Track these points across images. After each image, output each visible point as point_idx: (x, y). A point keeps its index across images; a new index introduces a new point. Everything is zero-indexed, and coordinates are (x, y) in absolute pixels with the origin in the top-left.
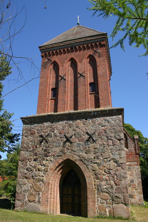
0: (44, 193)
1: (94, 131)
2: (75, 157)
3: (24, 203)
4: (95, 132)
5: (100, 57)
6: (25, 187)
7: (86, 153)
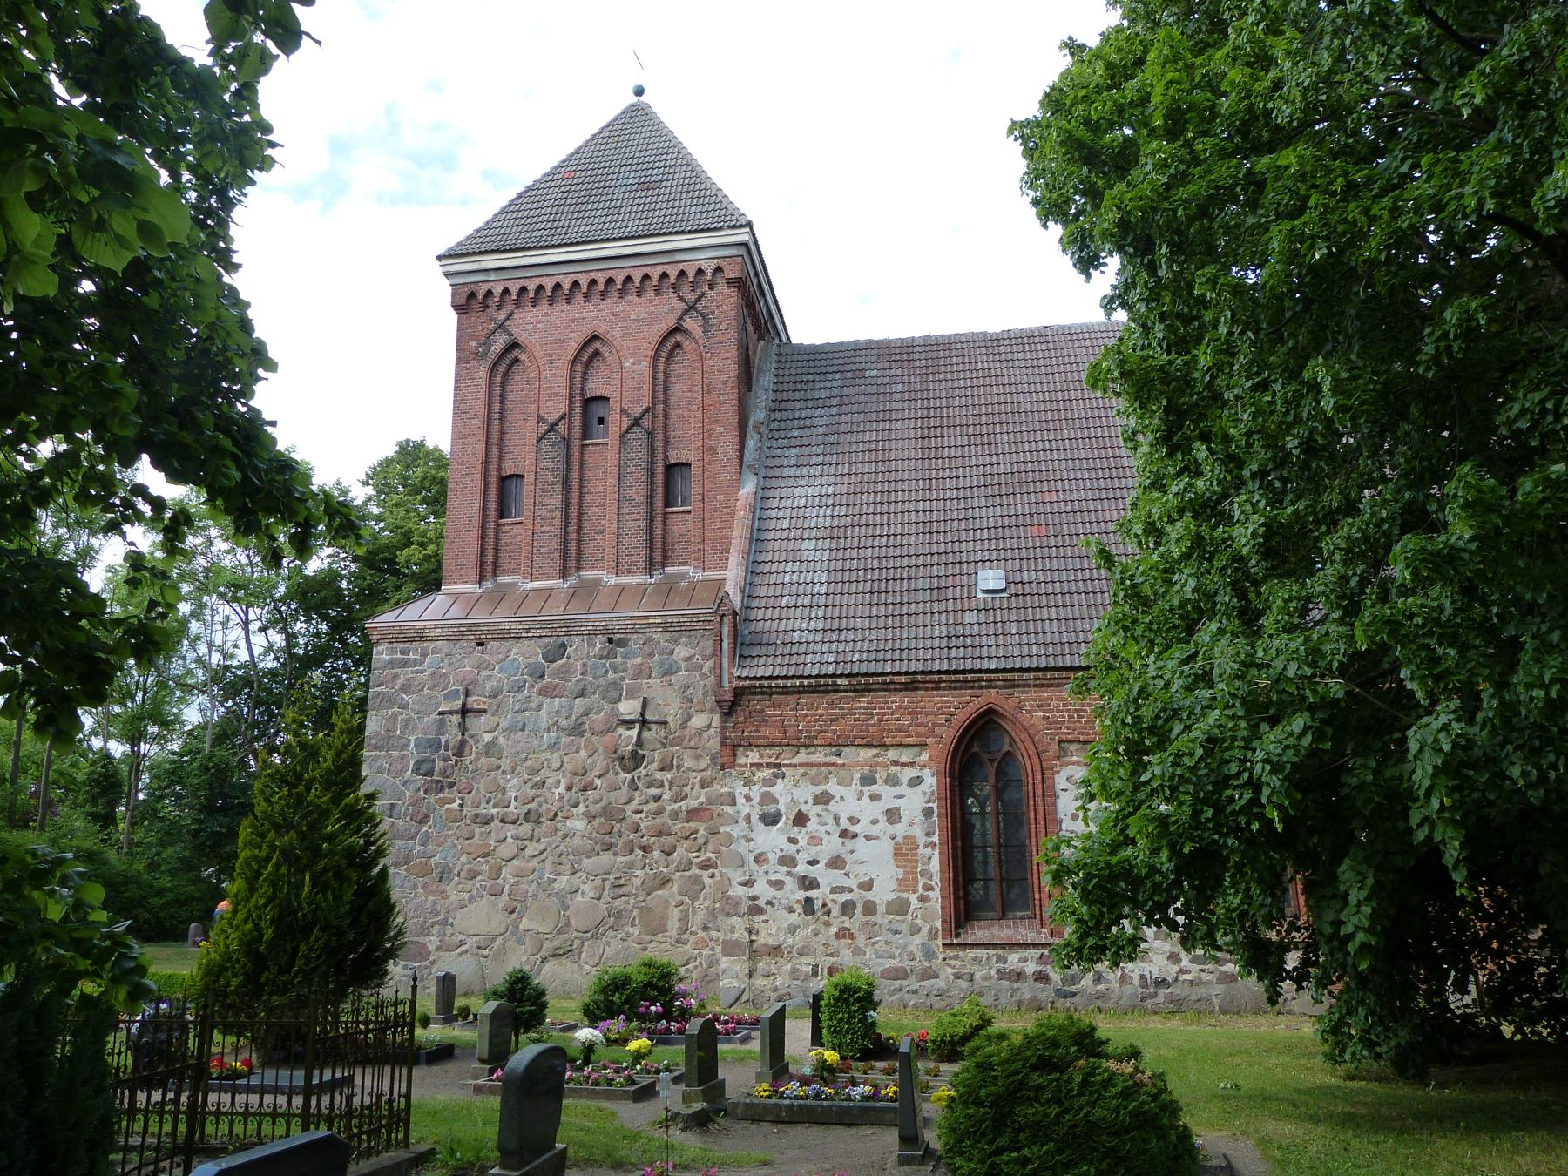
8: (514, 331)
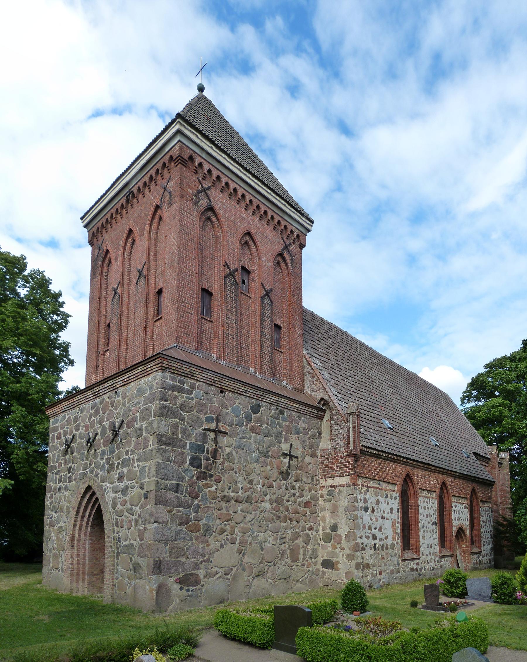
8: (212, 200)
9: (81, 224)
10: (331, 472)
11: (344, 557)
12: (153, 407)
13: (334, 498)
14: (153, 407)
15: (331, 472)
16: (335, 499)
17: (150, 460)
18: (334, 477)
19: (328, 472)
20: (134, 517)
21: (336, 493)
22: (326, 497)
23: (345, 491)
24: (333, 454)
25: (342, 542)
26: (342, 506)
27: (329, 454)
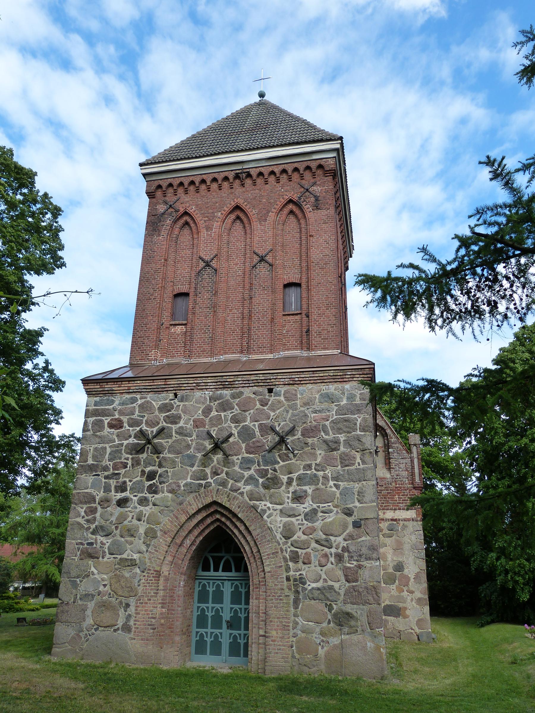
0: (141, 601)
1: (291, 425)
2: (235, 496)
3: (83, 631)
4: (294, 428)
5: (317, 207)
6: (85, 587)
7: (265, 487)
9: (138, 172)
10: (391, 503)
11: (414, 601)
12: (359, 420)
13: (396, 533)
14: (359, 420)
15: (391, 503)
16: (399, 534)
17: (360, 481)
18: (395, 510)
19: (387, 503)
20: (333, 550)
21: (400, 528)
22: (386, 531)
23: (411, 525)
24: (394, 484)
25: (410, 584)
26: (409, 543)
27: (388, 484)
